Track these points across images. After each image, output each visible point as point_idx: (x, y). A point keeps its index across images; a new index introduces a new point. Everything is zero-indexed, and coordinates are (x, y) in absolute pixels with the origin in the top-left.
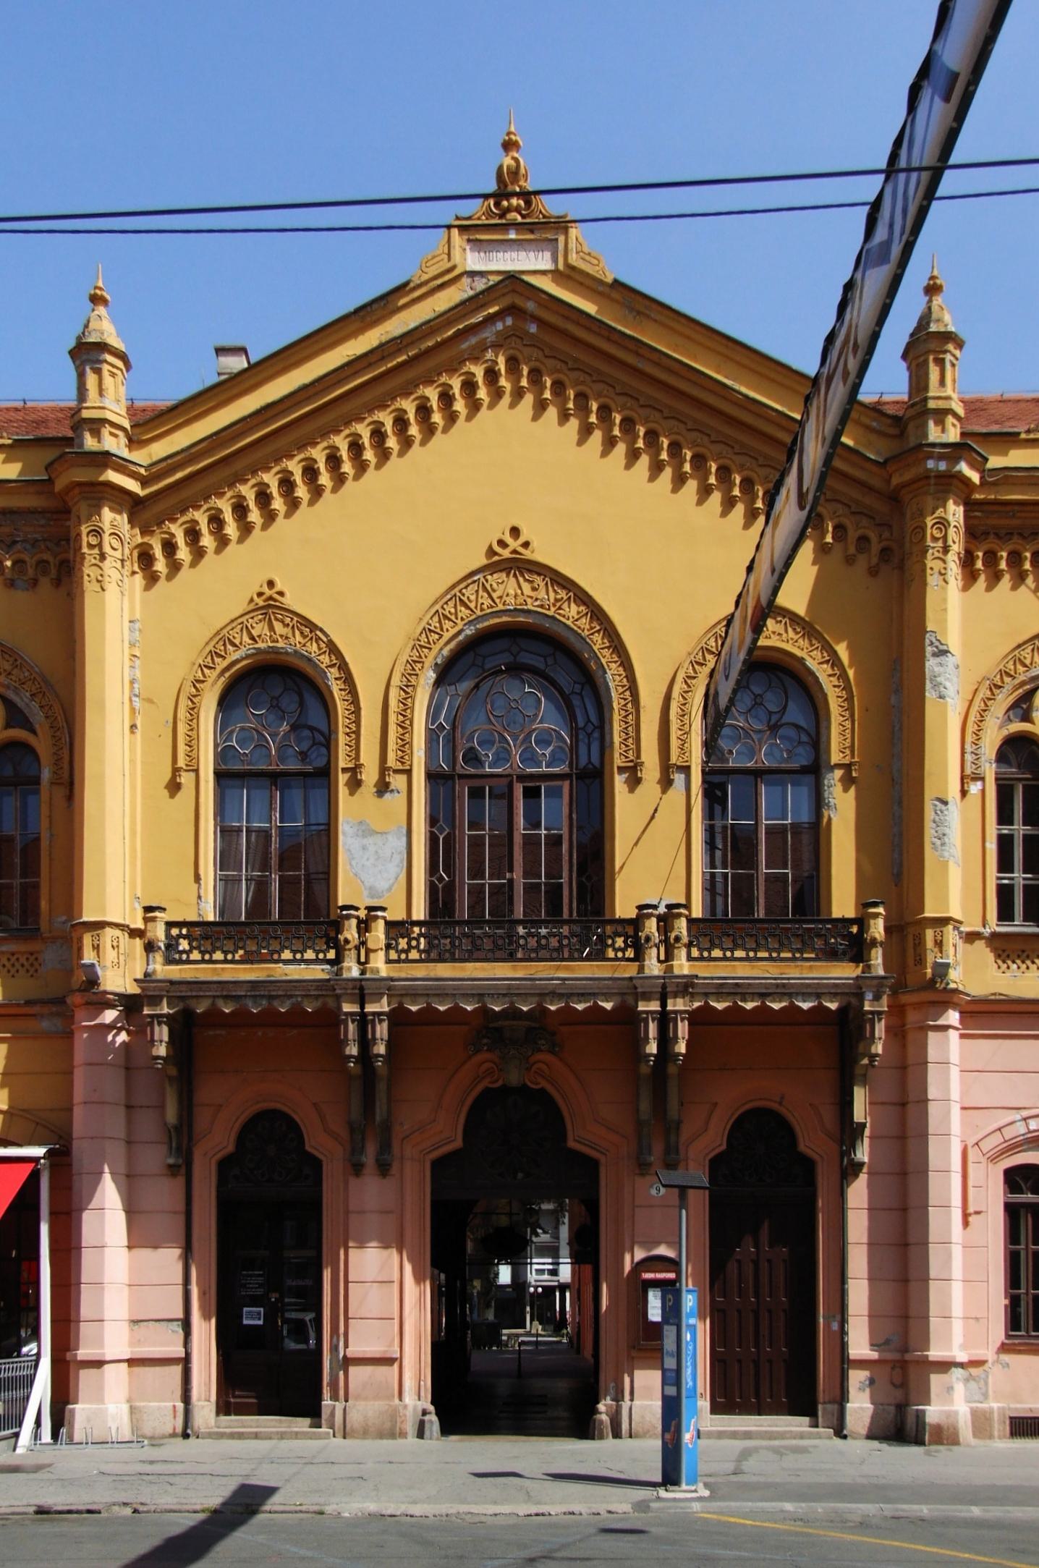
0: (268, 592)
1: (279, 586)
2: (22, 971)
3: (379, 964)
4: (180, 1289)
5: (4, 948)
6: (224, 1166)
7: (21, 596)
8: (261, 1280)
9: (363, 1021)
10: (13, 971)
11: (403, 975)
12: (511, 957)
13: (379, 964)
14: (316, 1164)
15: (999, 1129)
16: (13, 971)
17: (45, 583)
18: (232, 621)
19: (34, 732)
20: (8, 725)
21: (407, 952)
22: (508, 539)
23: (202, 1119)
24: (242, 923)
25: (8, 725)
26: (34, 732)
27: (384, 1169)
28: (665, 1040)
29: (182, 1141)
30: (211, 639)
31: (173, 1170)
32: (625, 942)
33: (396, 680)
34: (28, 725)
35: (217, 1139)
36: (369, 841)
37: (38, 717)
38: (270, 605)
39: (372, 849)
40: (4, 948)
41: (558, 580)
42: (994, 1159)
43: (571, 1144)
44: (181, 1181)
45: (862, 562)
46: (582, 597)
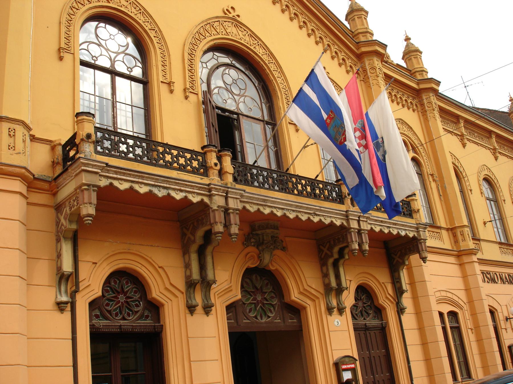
14: (155, 308)
29: (68, 280)
31: (60, 306)
35: (93, 283)
41: (253, 35)
44: (67, 315)
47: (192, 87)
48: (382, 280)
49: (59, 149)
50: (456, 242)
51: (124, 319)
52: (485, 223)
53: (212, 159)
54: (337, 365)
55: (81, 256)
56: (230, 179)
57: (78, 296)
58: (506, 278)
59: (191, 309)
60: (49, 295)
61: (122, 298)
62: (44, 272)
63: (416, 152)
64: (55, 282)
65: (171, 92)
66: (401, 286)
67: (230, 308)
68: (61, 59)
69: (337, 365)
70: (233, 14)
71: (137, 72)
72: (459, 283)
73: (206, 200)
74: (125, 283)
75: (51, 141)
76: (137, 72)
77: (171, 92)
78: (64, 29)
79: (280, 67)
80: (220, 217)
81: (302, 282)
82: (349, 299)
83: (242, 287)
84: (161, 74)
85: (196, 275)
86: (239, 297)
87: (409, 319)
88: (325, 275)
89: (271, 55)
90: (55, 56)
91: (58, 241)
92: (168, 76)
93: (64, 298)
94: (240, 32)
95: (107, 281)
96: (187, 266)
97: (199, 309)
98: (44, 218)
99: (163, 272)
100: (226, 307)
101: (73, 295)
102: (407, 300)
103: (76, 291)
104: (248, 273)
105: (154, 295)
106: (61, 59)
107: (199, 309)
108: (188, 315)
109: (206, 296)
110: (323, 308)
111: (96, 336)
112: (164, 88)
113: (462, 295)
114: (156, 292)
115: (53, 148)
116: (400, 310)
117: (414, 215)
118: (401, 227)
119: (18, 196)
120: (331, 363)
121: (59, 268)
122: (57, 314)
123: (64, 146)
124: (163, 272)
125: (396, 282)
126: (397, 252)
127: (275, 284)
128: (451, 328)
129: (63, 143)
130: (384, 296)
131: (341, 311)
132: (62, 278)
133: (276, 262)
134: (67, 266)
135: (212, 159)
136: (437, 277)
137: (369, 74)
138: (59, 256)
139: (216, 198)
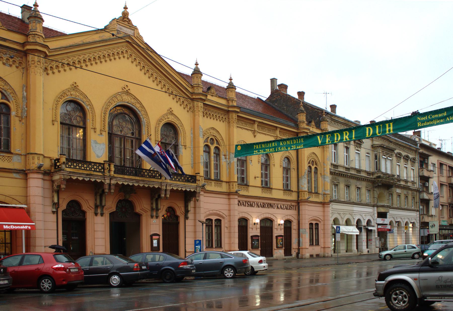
0: (75, 85)
1: (77, 84)
2: (6, 161)
4: (56, 239)
5: (2, 154)
6: (63, 211)
7: (7, 68)
14: (84, 213)
16: (3, 160)
17: (14, 66)
19: (9, 101)
20: (2, 99)
21: (86, 168)
22: (74, 84)
25: (2, 99)
26: (9, 101)
27: (102, 215)
28: (165, 194)
29: (56, 205)
31: (53, 212)
33: (103, 112)
35: (63, 206)
36: (97, 145)
38: (75, 87)
39: (98, 147)
40: (2, 154)
41: (135, 98)
44: (55, 215)
46: (141, 104)
47: (104, 129)
48: (179, 205)
49: (53, 161)
50: (229, 188)
51: (73, 216)
52: (255, 178)
53: (106, 166)
54: (151, 236)
55: (60, 197)
56: (112, 173)
57: (59, 209)
58: (261, 204)
59: (96, 214)
60: (50, 209)
61: (73, 209)
62: (48, 202)
63: (218, 144)
64: (52, 205)
65: (95, 132)
66: (188, 209)
67: (112, 214)
68: (53, 124)
69: (151, 236)
70: (127, 89)
71: (81, 124)
72: (227, 207)
73: (103, 181)
74: (74, 206)
75: (50, 157)
76: (81, 124)
77: (95, 132)
78: (54, 111)
79: (147, 113)
80: (107, 187)
81: (142, 206)
82: (162, 212)
83: (117, 205)
84: (91, 124)
85: (98, 203)
86: (115, 210)
87: (189, 222)
88: (152, 204)
89: (143, 107)
90: (51, 124)
91: (53, 192)
92: (94, 125)
93: (55, 210)
94: (129, 98)
95: (68, 204)
96: (96, 200)
97: (99, 214)
98: (48, 184)
99: (87, 202)
100: (110, 214)
101: (57, 209)
102: (190, 215)
103: (58, 208)
104: (120, 201)
105: (83, 209)
106: (53, 124)
107: (99, 214)
108: (95, 216)
109: (102, 210)
110: (149, 216)
111: (63, 220)
112: (92, 131)
113: (226, 213)
114: (84, 208)
115: (51, 160)
116: (186, 218)
117: (197, 182)
118: (190, 187)
119: (41, 180)
120: (149, 235)
121: (53, 201)
122: (52, 215)
123: (55, 160)
124: (87, 202)
125: (186, 207)
126: (188, 197)
127: (131, 205)
128: (215, 226)
129: (55, 159)
130: (180, 212)
131: (157, 217)
132: (54, 204)
133: (133, 198)
134: (56, 201)
135: (106, 166)
136: (209, 205)
137: (195, 109)
138: (53, 197)
139: (107, 180)
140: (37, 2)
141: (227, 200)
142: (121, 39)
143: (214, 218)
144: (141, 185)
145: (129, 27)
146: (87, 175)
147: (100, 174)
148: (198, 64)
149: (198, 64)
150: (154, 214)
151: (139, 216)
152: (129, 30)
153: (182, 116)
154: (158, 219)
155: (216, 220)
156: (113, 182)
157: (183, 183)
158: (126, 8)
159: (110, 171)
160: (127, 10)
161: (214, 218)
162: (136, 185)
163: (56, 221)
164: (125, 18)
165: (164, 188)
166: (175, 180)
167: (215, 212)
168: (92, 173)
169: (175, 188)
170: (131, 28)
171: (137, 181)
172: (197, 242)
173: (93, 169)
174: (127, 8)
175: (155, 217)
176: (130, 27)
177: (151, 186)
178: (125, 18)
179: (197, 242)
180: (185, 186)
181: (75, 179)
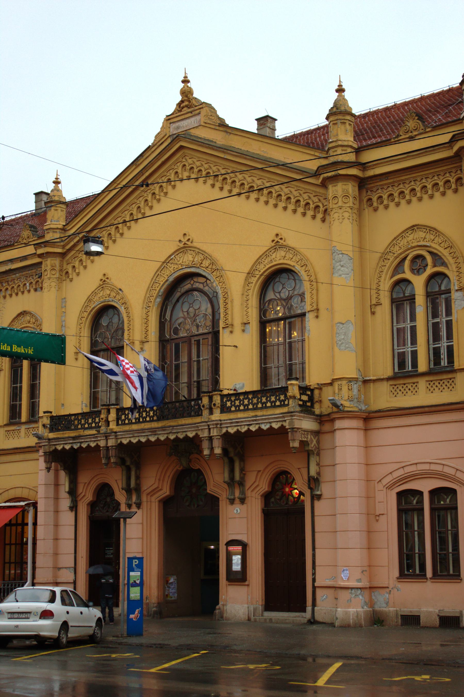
0: (276, 240)
3: (113, 426)
8: (112, 551)
9: (211, 439)
10: (405, 392)
11: (121, 430)
12: (190, 416)
13: (113, 426)
15: (457, 470)
17: (449, 192)
18: (93, 292)
23: (81, 489)
24: (174, 402)
30: (86, 301)
32: (266, 399)
34: (444, 264)
37: (449, 259)
42: (390, 487)
43: (208, 491)
44: (74, 513)
45: (449, 192)
82: (87, 495)
107: (237, 501)
140: (342, 84)
141: (362, 432)
142: (191, 145)
143: (425, 486)
144: (162, 438)
145: (190, 115)
146: (74, 438)
147: (94, 432)
148: (59, 183)
149: (59, 183)
150: (237, 493)
151: (214, 501)
152: (192, 119)
153: (302, 235)
154: (245, 505)
155: (433, 493)
156: (111, 442)
157: (252, 414)
158: (186, 81)
159: (108, 423)
160: (189, 85)
161: (425, 486)
162: (153, 439)
163: (73, 523)
164: (188, 103)
165: (205, 434)
166: (265, 407)
167: (426, 467)
168: (81, 432)
169: (232, 430)
170: (194, 113)
171: (153, 431)
172: (135, 562)
173: (278, 403)
174: (188, 82)
175: (237, 501)
176: (191, 112)
177: (181, 436)
178: (188, 103)
179: (135, 562)
180: (238, 423)
181: (246, 432)
